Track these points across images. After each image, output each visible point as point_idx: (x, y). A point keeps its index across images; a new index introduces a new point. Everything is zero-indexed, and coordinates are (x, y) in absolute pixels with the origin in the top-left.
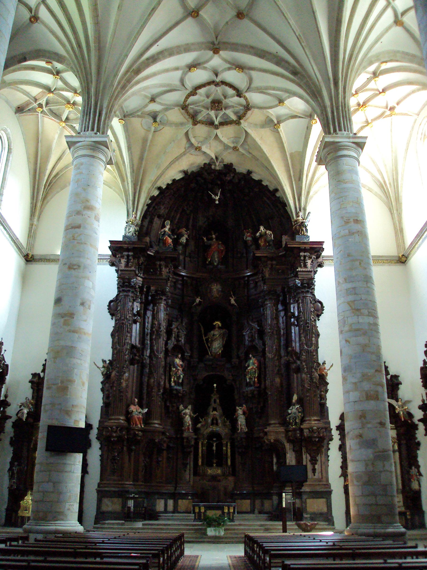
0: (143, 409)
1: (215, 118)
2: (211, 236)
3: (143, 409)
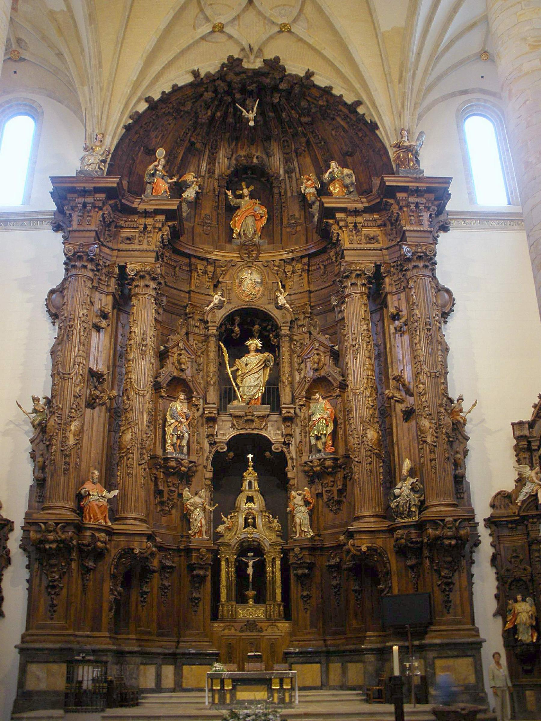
0: (109, 492)
2: (241, 192)
3: (109, 492)
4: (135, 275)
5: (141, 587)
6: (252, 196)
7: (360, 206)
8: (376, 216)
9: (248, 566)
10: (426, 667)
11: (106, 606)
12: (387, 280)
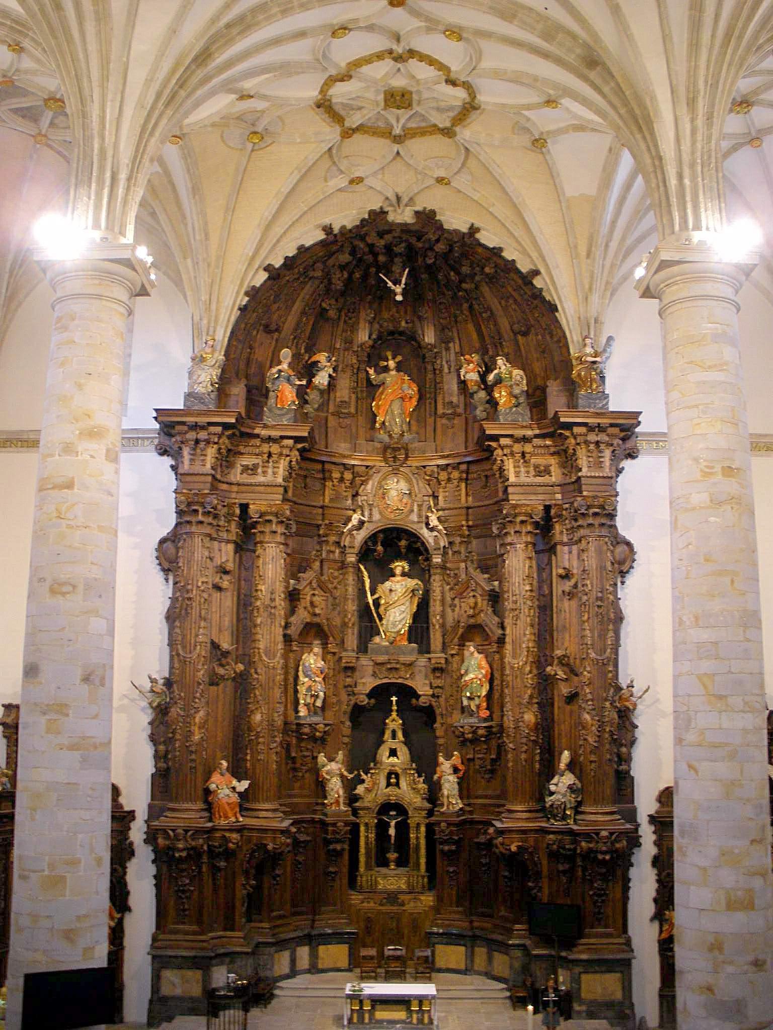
1: (395, 124)
2: (386, 363)
5: (274, 869)
6: (399, 368)
7: (529, 433)
8: (548, 442)
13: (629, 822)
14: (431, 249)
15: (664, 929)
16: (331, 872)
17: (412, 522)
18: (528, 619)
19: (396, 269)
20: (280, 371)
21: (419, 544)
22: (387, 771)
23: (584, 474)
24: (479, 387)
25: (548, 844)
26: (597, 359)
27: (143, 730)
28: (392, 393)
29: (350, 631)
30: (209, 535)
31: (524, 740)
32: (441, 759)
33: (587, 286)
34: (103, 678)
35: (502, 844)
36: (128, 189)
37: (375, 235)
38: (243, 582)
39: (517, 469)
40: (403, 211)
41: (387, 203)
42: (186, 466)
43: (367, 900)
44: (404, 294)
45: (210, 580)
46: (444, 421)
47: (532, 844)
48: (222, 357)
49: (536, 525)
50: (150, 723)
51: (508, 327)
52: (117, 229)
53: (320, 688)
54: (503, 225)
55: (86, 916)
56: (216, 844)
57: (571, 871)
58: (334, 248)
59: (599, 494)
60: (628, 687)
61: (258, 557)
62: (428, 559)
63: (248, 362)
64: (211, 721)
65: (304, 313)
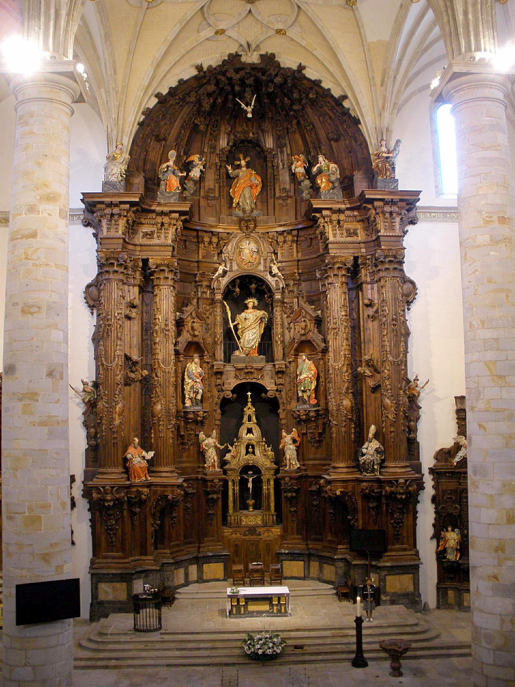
4: (156, 268)
5: (171, 514)
6: (248, 166)
7: (343, 206)
8: (356, 213)
9: (248, 482)
10: (379, 582)
11: (149, 537)
12: (363, 271)
13: (417, 473)
14: (272, 81)
15: (440, 544)
16: (211, 514)
17: (260, 271)
18: (345, 335)
19: (247, 95)
20: (168, 167)
21: (264, 286)
22: (246, 444)
23: (382, 234)
24: (305, 177)
25: (362, 489)
26: (390, 155)
27: (78, 419)
28: (244, 182)
29: (219, 347)
30: (122, 281)
31: (344, 418)
32: (284, 434)
33: (381, 106)
34: (62, 374)
35: (331, 490)
36: (68, 22)
37: (232, 71)
38: (145, 314)
39: (335, 232)
40: (252, 55)
41: (241, 49)
42: (105, 232)
43: (235, 532)
44: (253, 112)
45: (123, 312)
46: (281, 201)
47: (350, 489)
48: (127, 156)
49: (348, 269)
50: (83, 414)
51: (324, 135)
52: (61, 51)
53: (199, 386)
54: (322, 63)
55: (56, 544)
56: (133, 496)
57: (378, 508)
58: (204, 81)
59: (393, 248)
60: (414, 380)
61: (156, 295)
62: (271, 296)
63: (145, 161)
64: (126, 411)
65: (182, 127)
